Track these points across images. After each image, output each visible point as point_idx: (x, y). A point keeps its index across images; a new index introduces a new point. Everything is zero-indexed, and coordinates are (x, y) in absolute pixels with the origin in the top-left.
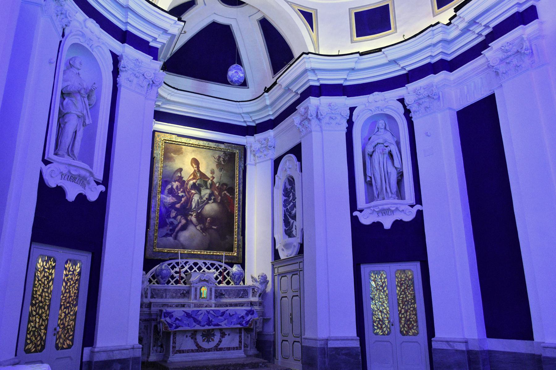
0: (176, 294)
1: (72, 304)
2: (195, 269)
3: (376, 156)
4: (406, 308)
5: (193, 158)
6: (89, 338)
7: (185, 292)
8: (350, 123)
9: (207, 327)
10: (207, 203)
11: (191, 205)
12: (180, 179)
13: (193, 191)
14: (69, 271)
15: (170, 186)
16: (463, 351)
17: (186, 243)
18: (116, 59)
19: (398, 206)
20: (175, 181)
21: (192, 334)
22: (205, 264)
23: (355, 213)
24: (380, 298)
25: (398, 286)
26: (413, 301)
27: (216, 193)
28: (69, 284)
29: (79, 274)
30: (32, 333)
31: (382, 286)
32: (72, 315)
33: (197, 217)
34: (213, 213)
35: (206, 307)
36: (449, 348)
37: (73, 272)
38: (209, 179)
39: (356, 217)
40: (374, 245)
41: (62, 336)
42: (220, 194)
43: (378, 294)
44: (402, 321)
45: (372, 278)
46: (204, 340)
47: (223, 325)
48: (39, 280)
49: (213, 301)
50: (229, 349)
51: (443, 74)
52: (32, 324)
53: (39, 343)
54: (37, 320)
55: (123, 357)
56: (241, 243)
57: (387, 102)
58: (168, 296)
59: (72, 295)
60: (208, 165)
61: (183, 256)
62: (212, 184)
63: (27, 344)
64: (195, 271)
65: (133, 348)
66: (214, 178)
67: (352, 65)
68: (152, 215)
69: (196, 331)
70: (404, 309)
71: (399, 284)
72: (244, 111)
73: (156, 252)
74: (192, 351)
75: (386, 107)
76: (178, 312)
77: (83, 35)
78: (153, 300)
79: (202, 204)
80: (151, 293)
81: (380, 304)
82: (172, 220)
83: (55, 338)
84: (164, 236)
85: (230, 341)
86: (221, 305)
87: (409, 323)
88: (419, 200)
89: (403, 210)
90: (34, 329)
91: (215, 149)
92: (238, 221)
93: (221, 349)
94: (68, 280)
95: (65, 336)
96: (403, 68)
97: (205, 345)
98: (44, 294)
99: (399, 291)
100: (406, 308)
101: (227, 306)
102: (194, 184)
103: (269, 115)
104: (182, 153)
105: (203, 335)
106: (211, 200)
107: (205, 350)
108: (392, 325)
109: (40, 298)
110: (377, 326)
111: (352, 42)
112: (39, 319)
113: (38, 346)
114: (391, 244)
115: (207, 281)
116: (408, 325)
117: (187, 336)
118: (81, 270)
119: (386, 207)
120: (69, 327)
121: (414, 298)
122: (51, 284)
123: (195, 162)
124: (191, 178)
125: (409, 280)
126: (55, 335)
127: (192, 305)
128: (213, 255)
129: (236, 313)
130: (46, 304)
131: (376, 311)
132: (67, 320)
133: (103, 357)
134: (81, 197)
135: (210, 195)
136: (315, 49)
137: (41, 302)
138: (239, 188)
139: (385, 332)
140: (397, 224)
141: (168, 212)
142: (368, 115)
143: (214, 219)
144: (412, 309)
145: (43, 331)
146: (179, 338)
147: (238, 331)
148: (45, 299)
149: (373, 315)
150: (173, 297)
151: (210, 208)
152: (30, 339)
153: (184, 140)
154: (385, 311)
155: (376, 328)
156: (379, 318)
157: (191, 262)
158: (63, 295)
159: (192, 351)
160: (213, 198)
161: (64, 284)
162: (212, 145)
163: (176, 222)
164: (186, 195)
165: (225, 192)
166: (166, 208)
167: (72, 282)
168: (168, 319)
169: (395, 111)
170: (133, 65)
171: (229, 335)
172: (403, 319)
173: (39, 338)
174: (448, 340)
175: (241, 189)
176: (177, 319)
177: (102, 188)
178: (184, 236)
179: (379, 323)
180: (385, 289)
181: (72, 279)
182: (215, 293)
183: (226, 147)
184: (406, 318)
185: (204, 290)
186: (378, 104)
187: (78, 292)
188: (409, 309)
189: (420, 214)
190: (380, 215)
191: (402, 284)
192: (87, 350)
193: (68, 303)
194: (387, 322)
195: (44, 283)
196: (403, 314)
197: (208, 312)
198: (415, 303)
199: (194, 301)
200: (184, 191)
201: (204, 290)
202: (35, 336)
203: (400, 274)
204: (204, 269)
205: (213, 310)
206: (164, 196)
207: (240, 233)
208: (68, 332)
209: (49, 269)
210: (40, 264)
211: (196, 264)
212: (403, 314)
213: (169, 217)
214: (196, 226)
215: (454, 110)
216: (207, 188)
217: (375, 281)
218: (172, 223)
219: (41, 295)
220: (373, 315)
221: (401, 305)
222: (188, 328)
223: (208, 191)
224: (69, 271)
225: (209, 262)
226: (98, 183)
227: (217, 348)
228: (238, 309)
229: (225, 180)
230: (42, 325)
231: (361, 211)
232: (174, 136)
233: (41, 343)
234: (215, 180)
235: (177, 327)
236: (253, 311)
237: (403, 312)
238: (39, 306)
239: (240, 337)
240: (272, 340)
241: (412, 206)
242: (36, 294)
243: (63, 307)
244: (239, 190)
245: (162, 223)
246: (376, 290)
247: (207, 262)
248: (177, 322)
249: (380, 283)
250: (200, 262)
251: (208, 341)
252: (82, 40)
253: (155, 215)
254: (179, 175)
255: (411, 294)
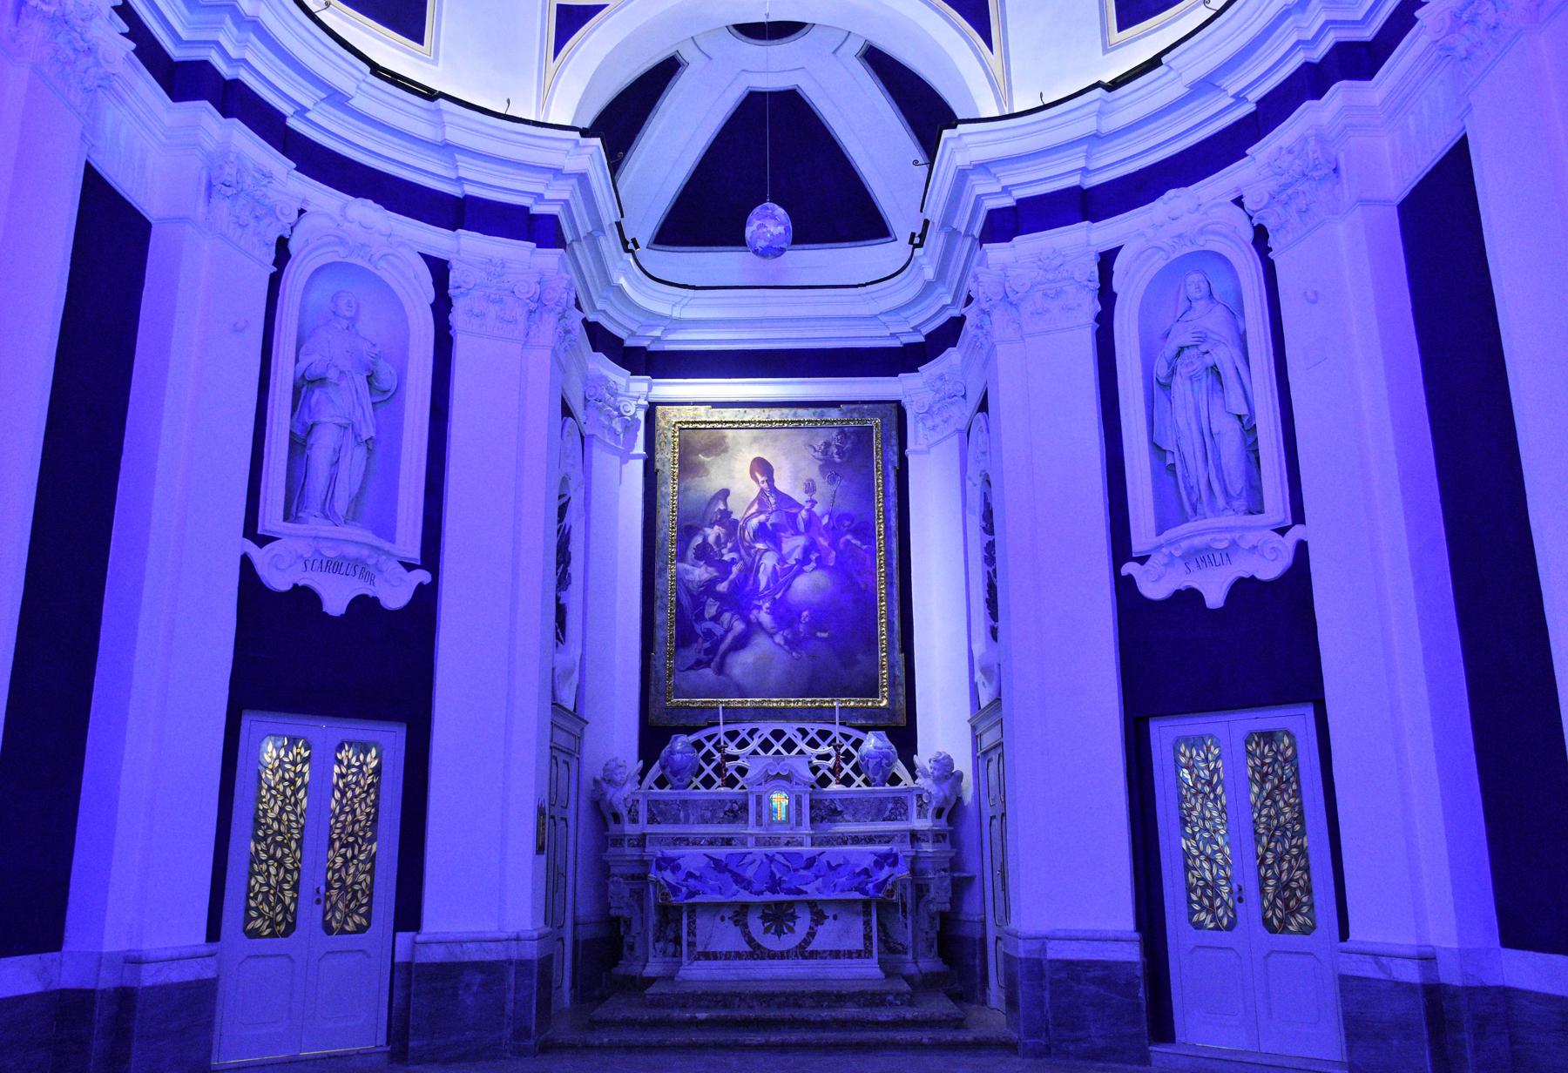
0: (714, 811)
1: (363, 838)
2: (778, 746)
3: (1180, 386)
4: (1279, 849)
5: (753, 455)
6: (408, 913)
7: (736, 807)
8: (1107, 296)
9: (768, 897)
10: (800, 572)
11: (757, 582)
12: (725, 518)
13: (760, 546)
14: (349, 766)
15: (698, 540)
16: (1410, 987)
17: (747, 682)
18: (439, 269)
19: (1236, 535)
20: (711, 525)
21: (737, 914)
22: (804, 733)
23: (1129, 568)
24: (1204, 819)
25: (1252, 780)
26: (1297, 827)
27: (823, 542)
28: (349, 794)
29: (377, 771)
30: (260, 897)
31: (1209, 783)
32: (363, 862)
33: (772, 611)
34: (815, 599)
35: (787, 844)
36: (1382, 976)
37: (360, 767)
38: (801, 507)
39: (1130, 578)
40: (1215, 654)
41: (341, 905)
42: (833, 544)
43: (1198, 807)
44: (1269, 890)
45: (1183, 760)
46: (767, 930)
47: (812, 891)
48: (270, 788)
49: (806, 830)
50: (836, 954)
51: (1340, 93)
52: (260, 878)
53: (280, 918)
54: (273, 871)
55: (488, 958)
56: (900, 673)
57: (1205, 213)
58: (692, 818)
59: (362, 818)
60: (796, 472)
61: (734, 715)
62: (811, 521)
63: (249, 919)
64: (778, 752)
65: (518, 939)
66: (814, 503)
67: (1088, 126)
68: (659, 617)
69: (745, 907)
70: (1274, 851)
71: (1257, 776)
72: (884, 309)
73: (673, 709)
74: (739, 956)
75: (1202, 232)
76: (692, 858)
77: (342, 242)
78: (651, 829)
79: (784, 577)
80: (649, 810)
81: (1206, 835)
82: (709, 625)
83: (320, 908)
84: (690, 668)
85: (834, 933)
86: (829, 841)
87: (1287, 894)
88: (1298, 516)
89: (1255, 547)
90: (265, 889)
91: (813, 426)
92: (890, 612)
93: (813, 955)
94: (347, 785)
95: (347, 906)
96: (1239, 98)
97: (770, 942)
98: (285, 817)
99: (1258, 796)
100: (1279, 849)
101: (845, 843)
102: (762, 525)
103: (944, 307)
104: (725, 450)
105: (765, 918)
106: (809, 561)
107: (773, 955)
108: (1240, 900)
109: (276, 826)
110: (1200, 902)
111: (1106, 51)
112: (277, 869)
113: (279, 924)
114: (1215, 654)
115: (788, 778)
116: (1286, 902)
117: (722, 919)
118: (379, 764)
119: (1197, 542)
120: (357, 887)
121: (1300, 819)
122: (301, 794)
123: (762, 467)
124: (753, 510)
125: (1286, 760)
126: (318, 902)
127: (751, 841)
128: (820, 708)
129: (847, 862)
130: (291, 839)
131: (1195, 857)
132: (352, 870)
133: (437, 955)
134: (364, 606)
135: (807, 551)
136: (998, 101)
137: (279, 833)
138: (887, 521)
139: (1221, 920)
140: (1243, 588)
141: (699, 606)
142: (1159, 262)
143: (822, 614)
144: (1295, 851)
145: (289, 894)
146: (703, 922)
147: (860, 908)
148: (289, 828)
149: (1187, 868)
150: (705, 821)
151: (809, 585)
152: (256, 909)
153: (729, 414)
154: (1219, 856)
155: (1197, 907)
156: (1204, 879)
157: (766, 729)
158: (337, 818)
159: (739, 956)
160: (813, 557)
161: (337, 795)
162: (805, 414)
163: (718, 630)
164: (741, 558)
165: (849, 537)
166: (692, 596)
167: (358, 791)
168: (668, 875)
169: (1225, 237)
170: (483, 274)
171: (835, 918)
172: (1271, 882)
173: (278, 908)
174: (1377, 949)
175: (894, 523)
176: (690, 875)
177: (424, 576)
178: (743, 663)
179: (1204, 893)
180: (1219, 790)
181: (357, 783)
182: (811, 808)
183: (844, 414)
184: (1278, 879)
185: (780, 801)
186: (1178, 227)
187: (376, 813)
188: (1288, 852)
189: (1302, 548)
190: (1193, 566)
191: (1264, 776)
192: (403, 938)
193: (350, 835)
194: (1226, 889)
195: (284, 794)
196: (1270, 867)
197: (771, 858)
198: (1302, 834)
199: (756, 831)
200: (735, 549)
201: (780, 801)
202: (269, 903)
203: (1258, 744)
204: (802, 745)
205: (783, 854)
206: (685, 566)
207: (898, 645)
208: (354, 897)
209: (294, 763)
210: (270, 752)
211: (778, 734)
212: (1270, 867)
213: (700, 617)
214: (771, 636)
215: (1386, 202)
216: (797, 533)
217: (1190, 769)
218: (709, 634)
219: (278, 819)
220: (1187, 868)
221: (1265, 839)
222: (718, 898)
223: (801, 541)
224: (349, 766)
225: (813, 728)
226: (409, 567)
227: (803, 952)
228: (851, 852)
229: (845, 506)
230: (285, 881)
231: (1142, 560)
232: (702, 408)
233: (284, 918)
234: (817, 509)
235: (691, 894)
236: (896, 856)
237: (1269, 861)
238: (274, 841)
239: (867, 923)
240: (978, 936)
241: (1282, 531)
242: (265, 816)
243: (337, 844)
244: (887, 528)
245: (685, 636)
246: (1195, 795)
247: (807, 727)
248: (691, 881)
249: (1205, 774)
250: (790, 729)
251: (779, 933)
252: (342, 251)
253: (665, 617)
254: (722, 507)
255: (1292, 806)
